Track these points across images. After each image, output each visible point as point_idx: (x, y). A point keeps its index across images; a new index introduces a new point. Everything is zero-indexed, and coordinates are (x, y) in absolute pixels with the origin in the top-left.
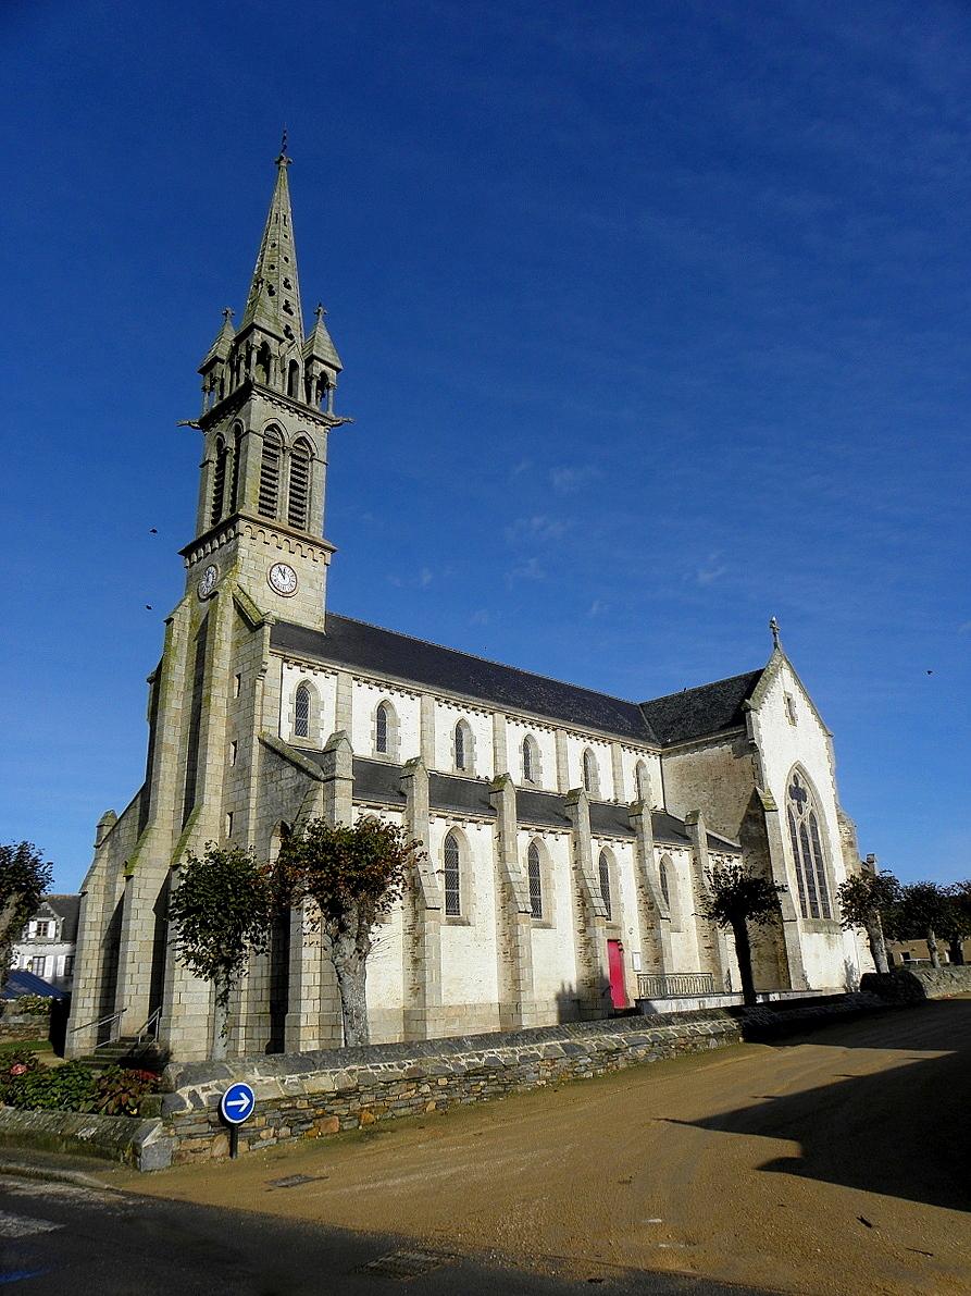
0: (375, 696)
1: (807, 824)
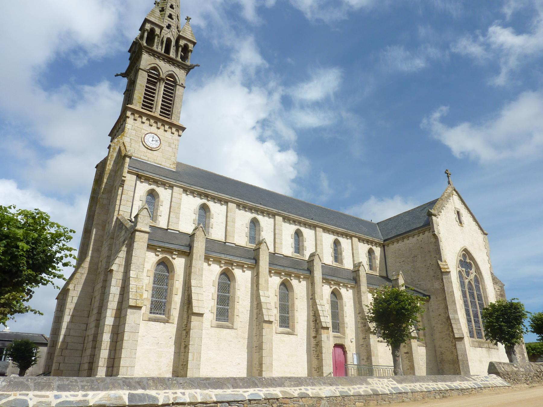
0: (249, 216)
1: (473, 283)
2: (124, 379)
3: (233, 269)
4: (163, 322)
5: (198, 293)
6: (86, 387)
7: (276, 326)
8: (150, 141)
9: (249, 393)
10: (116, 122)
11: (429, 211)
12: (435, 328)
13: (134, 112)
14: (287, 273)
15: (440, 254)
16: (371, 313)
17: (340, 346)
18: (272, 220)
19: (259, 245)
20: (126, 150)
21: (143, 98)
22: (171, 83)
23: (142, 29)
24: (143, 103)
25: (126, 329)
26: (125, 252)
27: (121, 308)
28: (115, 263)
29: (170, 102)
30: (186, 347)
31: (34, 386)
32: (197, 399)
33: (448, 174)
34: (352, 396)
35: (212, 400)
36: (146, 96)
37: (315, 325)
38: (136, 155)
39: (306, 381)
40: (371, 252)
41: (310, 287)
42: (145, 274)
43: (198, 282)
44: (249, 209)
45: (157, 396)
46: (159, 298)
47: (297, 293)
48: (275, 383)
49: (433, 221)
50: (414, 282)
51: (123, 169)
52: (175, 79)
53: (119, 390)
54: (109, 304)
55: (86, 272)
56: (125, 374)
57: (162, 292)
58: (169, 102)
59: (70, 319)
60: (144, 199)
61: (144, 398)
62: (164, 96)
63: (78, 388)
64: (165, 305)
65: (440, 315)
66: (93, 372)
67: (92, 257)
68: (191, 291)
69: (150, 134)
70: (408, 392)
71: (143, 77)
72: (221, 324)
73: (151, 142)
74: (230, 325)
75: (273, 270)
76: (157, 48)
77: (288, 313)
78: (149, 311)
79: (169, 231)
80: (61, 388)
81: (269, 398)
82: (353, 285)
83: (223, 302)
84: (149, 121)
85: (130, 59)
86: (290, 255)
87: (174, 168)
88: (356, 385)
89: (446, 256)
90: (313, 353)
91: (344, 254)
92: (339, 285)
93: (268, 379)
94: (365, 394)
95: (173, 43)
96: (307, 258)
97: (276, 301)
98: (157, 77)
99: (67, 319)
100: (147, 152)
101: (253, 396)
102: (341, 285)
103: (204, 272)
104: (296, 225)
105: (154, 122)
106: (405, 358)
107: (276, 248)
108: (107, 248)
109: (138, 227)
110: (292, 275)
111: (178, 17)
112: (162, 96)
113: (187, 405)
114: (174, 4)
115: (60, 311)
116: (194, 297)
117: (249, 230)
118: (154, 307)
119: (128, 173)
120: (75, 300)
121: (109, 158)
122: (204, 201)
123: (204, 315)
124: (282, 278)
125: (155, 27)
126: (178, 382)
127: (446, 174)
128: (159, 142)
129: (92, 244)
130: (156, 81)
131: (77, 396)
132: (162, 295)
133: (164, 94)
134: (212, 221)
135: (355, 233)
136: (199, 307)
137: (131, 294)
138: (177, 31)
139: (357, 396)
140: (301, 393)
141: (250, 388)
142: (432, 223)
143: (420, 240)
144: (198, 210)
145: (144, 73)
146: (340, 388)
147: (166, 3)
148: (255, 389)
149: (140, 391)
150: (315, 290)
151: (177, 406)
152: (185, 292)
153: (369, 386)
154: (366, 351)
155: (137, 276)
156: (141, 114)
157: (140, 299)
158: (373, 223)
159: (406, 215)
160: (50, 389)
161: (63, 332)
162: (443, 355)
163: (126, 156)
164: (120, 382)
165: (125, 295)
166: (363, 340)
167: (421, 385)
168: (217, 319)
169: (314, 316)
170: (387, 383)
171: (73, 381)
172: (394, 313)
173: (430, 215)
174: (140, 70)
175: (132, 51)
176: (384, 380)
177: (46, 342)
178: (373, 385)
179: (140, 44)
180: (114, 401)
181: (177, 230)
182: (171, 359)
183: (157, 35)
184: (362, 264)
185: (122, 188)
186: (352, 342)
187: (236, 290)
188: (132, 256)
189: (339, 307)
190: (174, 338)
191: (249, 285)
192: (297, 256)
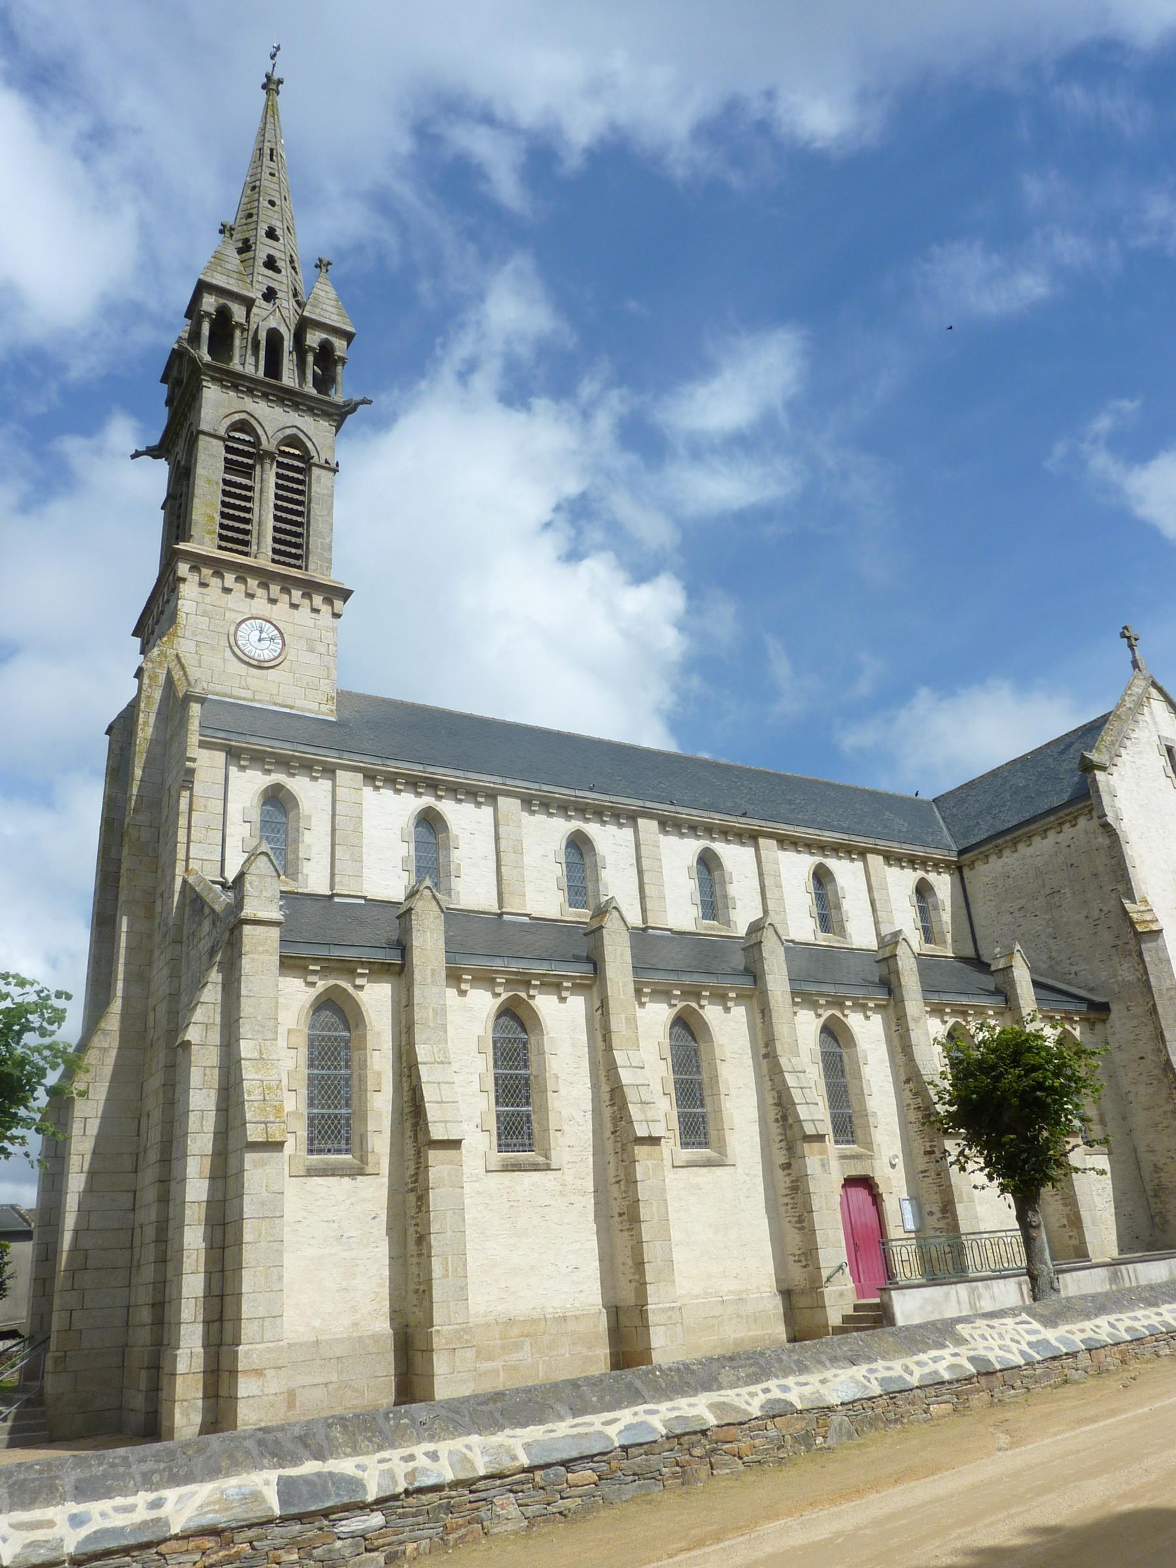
0: (561, 827)
2: (260, 1434)
3: (532, 997)
4: (349, 1176)
5: (438, 1080)
6: (156, 1478)
7: (671, 1147)
8: (253, 641)
9: (619, 1426)
10: (149, 595)
11: (1083, 758)
12: (1131, 1097)
13: (198, 562)
14: (686, 989)
15: (1128, 881)
16: (944, 1104)
17: (864, 1183)
18: (628, 832)
19: (598, 919)
20: (187, 679)
21: (218, 517)
22: (296, 463)
23: (193, 311)
24: (221, 531)
25: (245, 1210)
26: (219, 988)
27: (227, 1150)
28: (193, 1020)
29: (299, 519)
30: (422, 1239)
31: (10, 1497)
32: (474, 1469)
33: (1129, 638)
34: (917, 1387)
35: (517, 1464)
36: (226, 510)
37: (782, 1132)
38: (218, 688)
39: (780, 1360)
40: (923, 891)
41: (759, 1021)
42: (282, 1042)
43: (436, 1049)
44: (559, 808)
45: (359, 1474)
46: (329, 1107)
47: (722, 1045)
48: (692, 1382)
49: (1100, 785)
50: (1058, 968)
51: (187, 736)
52: (306, 450)
53: (249, 1473)
54: (189, 1142)
55: (116, 1044)
56: (258, 1339)
57: (336, 1088)
58: (295, 486)
59: (87, 1182)
60: (256, 816)
61: (324, 1487)
62: (280, 503)
63: (132, 1482)
64: (348, 1125)
65: (1142, 1058)
66: (166, 1329)
67: (126, 999)
68: (419, 1077)
69: (252, 621)
70: (1078, 1352)
71: (212, 456)
72: (513, 1161)
73: (257, 644)
74: (541, 1160)
75: (647, 984)
76: (243, 364)
77: (702, 1106)
78: (305, 1147)
79: (337, 899)
80: (86, 1491)
81: (678, 1432)
82: (882, 999)
83: (512, 1096)
84: (245, 582)
85: (169, 402)
86: (691, 928)
87: (332, 711)
88: (924, 1352)
89: (1145, 883)
90: (787, 1212)
91: (846, 905)
92: (841, 1005)
93: (670, 1369)
94: (954, 1377)
95: (288, 343)
96: (741, 930)
97: (665, 1074)
98: (252, 450)
99: (76, 1183)
100: (247, 675)
101: (633, 1432)
102: (849, 1003)
103: (450, 1017)
104: (698, 837)
105: (259, 586)
106: (1052, 1196)
107: (648, 913)
108: (166, 972)
109: (248, 911)
110: (704, 993)
111: (292, 261)
112: (272, 505)
113: (447, 1489)
114: (277, 224)
115: (56, 1156)
116: (429, 1093)
117: (564, 869)
118: (320, 1132)
119: (200, 747)
120: (93, 1127)
121: (142, 705)
122: (427, 800)
123: (463, 1142)
124: (675, 1005)
125: (230, 304)
126: (413, 1420)
127: (1126, 639)
128: (280, 641)
129: (122, 960)
130: (250, 462)
131: (130, 1509)
132: (336, 1097)
133: (277, 497)
134: (455, 855)
135: (872, 841)
136: (446, 1122)
137: (250, 1108)
138: (295, 304)
139: (931, 1385)
140: (769, 1401)
141: (621, 1408)
142: (1097, 791)
143: (1064, 844)
144: (413, 829)
145: (215, 441)
146: (880, 1368)
147: (253, 226)
148: (636, 1409)
149: (310, 1467)
150: (775, 1029)
151: (420, 1496)
152: (401, 1081)
153: (962, 1350)
154: (936, 1189)
155: (261, 1053)
156: (219, 567)
157: (278, 1120)
158: (923, 801)
159: (1017, 771)
160: (53, 1498)
161: (70, 1221)
162: (1162, 1174)
163: (188, 698)
164: (250, 1444)
165: (231, 1111)
166: (926, 1158)
167: (1112, 1321)
168: (499, 1145)
169: (779, 1104)
170: (1014, 1329)
171: (117, 1461)
172: (1015, 1101)
173: (1088, 767)
174: (201, 437)
175: (170, 380)
176: (1004, 1321)
177: (23, 1227)
178: (973, 1344)
179: (193, 360)
180: (239, 1510)
181: (359, 894)
182: (382, 1279)
183: (239, 325)
184: (901, 937)
185: (188, 792)
186: (893, 1166)
187: (547, 1056)
188: (239, 996)
189: (847, 1068)
190: (383, 1217)
191: (583, 1038)
192: (712, 928)
